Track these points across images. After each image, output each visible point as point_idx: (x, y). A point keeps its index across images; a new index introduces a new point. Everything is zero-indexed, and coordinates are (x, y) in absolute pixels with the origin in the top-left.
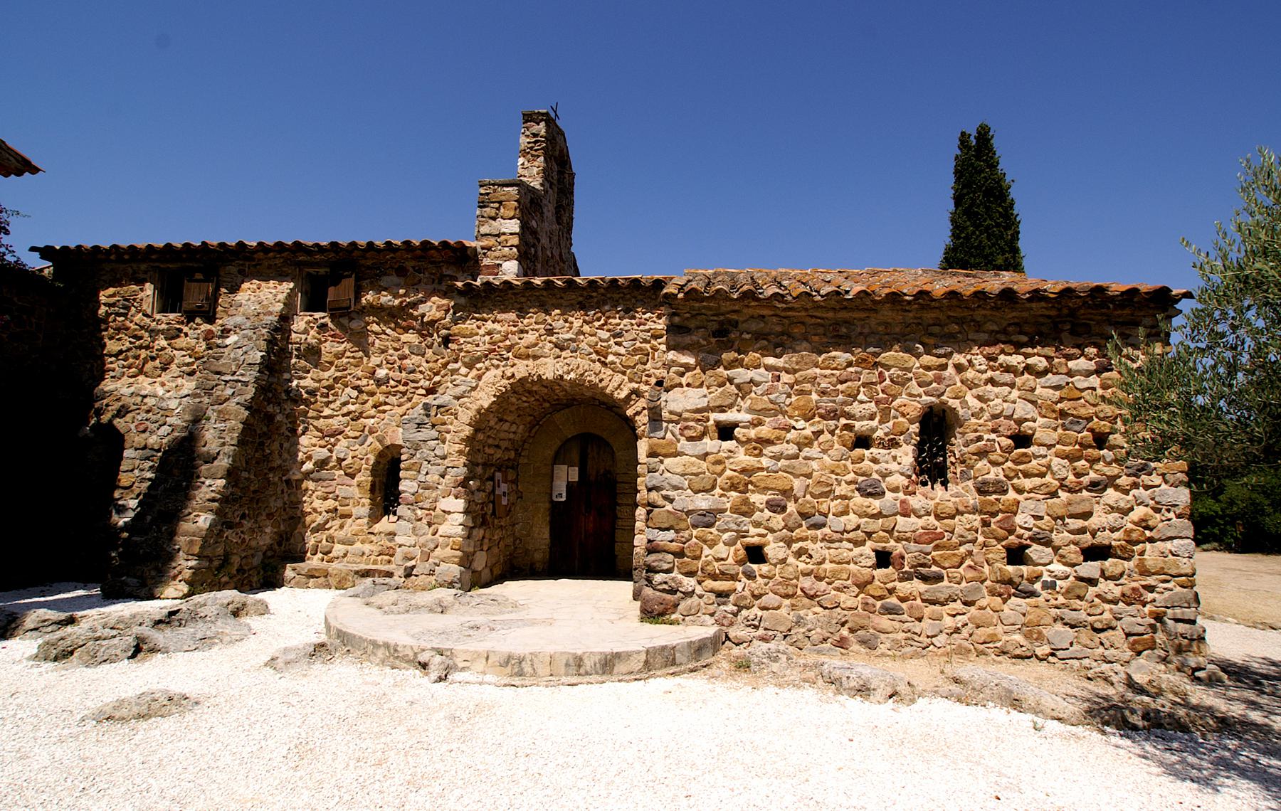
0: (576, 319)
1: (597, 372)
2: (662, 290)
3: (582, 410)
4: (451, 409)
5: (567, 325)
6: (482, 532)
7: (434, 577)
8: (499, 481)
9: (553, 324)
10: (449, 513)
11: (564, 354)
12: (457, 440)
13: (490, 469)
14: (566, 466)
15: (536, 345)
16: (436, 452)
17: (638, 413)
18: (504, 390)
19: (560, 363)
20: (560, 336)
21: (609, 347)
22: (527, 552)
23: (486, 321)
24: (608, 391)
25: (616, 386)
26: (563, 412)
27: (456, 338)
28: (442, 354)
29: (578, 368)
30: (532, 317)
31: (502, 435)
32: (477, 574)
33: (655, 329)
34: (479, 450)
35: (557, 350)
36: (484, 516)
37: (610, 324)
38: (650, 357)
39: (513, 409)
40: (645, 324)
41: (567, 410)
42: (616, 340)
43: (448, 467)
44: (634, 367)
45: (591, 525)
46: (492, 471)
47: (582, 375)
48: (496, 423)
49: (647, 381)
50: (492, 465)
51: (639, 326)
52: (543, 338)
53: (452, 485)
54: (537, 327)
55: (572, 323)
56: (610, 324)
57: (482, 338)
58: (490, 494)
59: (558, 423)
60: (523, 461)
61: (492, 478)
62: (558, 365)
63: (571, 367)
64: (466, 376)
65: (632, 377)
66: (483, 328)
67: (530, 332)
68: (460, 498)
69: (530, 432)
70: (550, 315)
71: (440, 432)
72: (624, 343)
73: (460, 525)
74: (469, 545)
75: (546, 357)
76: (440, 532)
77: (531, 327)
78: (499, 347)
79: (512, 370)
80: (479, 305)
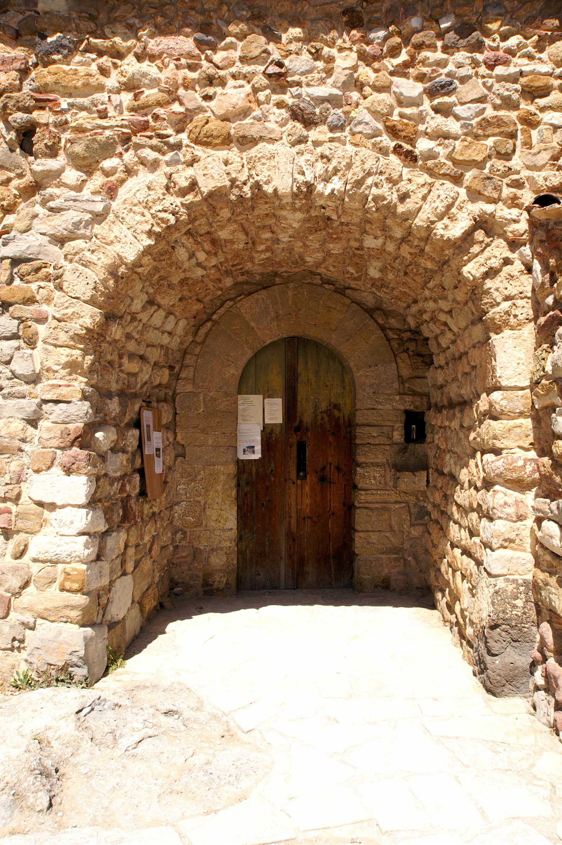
0: (341, 50)
1: (395, 176)
2: (486, 37)
3: (290, 293)
4: (45, 266)
5: (320, 64)
6: (123, 536)
7: (24, 654)
8: (148, 426)
9: (286, 62)
10: (52, 507)
11: (314, 134)
12: (63, 338)
13: (133, 404)
14: (261, 397)
15: (245, 113)
16: (13, 366)
17: (492, 273)
18: (172, 220)
19: (307, 156)
20: (305, 90)
21: (421, 118)
22: (196, 553)
23: (119, 55)
24: (419, 221)
25: (441, 208)
26: (255, 296)
27: (52, 96)
28: (19, 167)
29: (349, 166)
30: (231, 47)
31: (152, 336)
32: (118, 628)
33: (532, 72)
34: (110, 363)
35: (299, 125)
36: (125, 502)
37: (423, 62)
38: (518, 143)
39: (175, 280)
40: (506, 63)
41: (263, 294)
42: (436, 102)
43: (46, 402)
44: (480, 165)
45: (308, 501)
46: (137, 407)
47: (359, 183)
48: (144, 308)
49: (515, 198)
50: (135, 396)
51: (491, 67)
52: (262, 96)
53: (55, 443)
54: (246, 69)
55: (330, 60)
56: (423, 62)
57: (114, 97)
58: (134, 454)
59: (247, 317)
60: (184, 387)
61: (137, 424)
62: (301, 161)
63: (334, 163)
64: (79, 188)
65: (479, 187)
66: (114, 73)
67: (231, 82)
68: (78, 472)
69: (195, 334)
70: (277, 39)
71: (21, 320)
72: (459, 110)
73: (84, 534)
74: (101, 575)
75: (272, 141)
76: (31, 553)
77: (233, 70)
78: (156, 117)
79: (190, 172)
80: (103, 17)
